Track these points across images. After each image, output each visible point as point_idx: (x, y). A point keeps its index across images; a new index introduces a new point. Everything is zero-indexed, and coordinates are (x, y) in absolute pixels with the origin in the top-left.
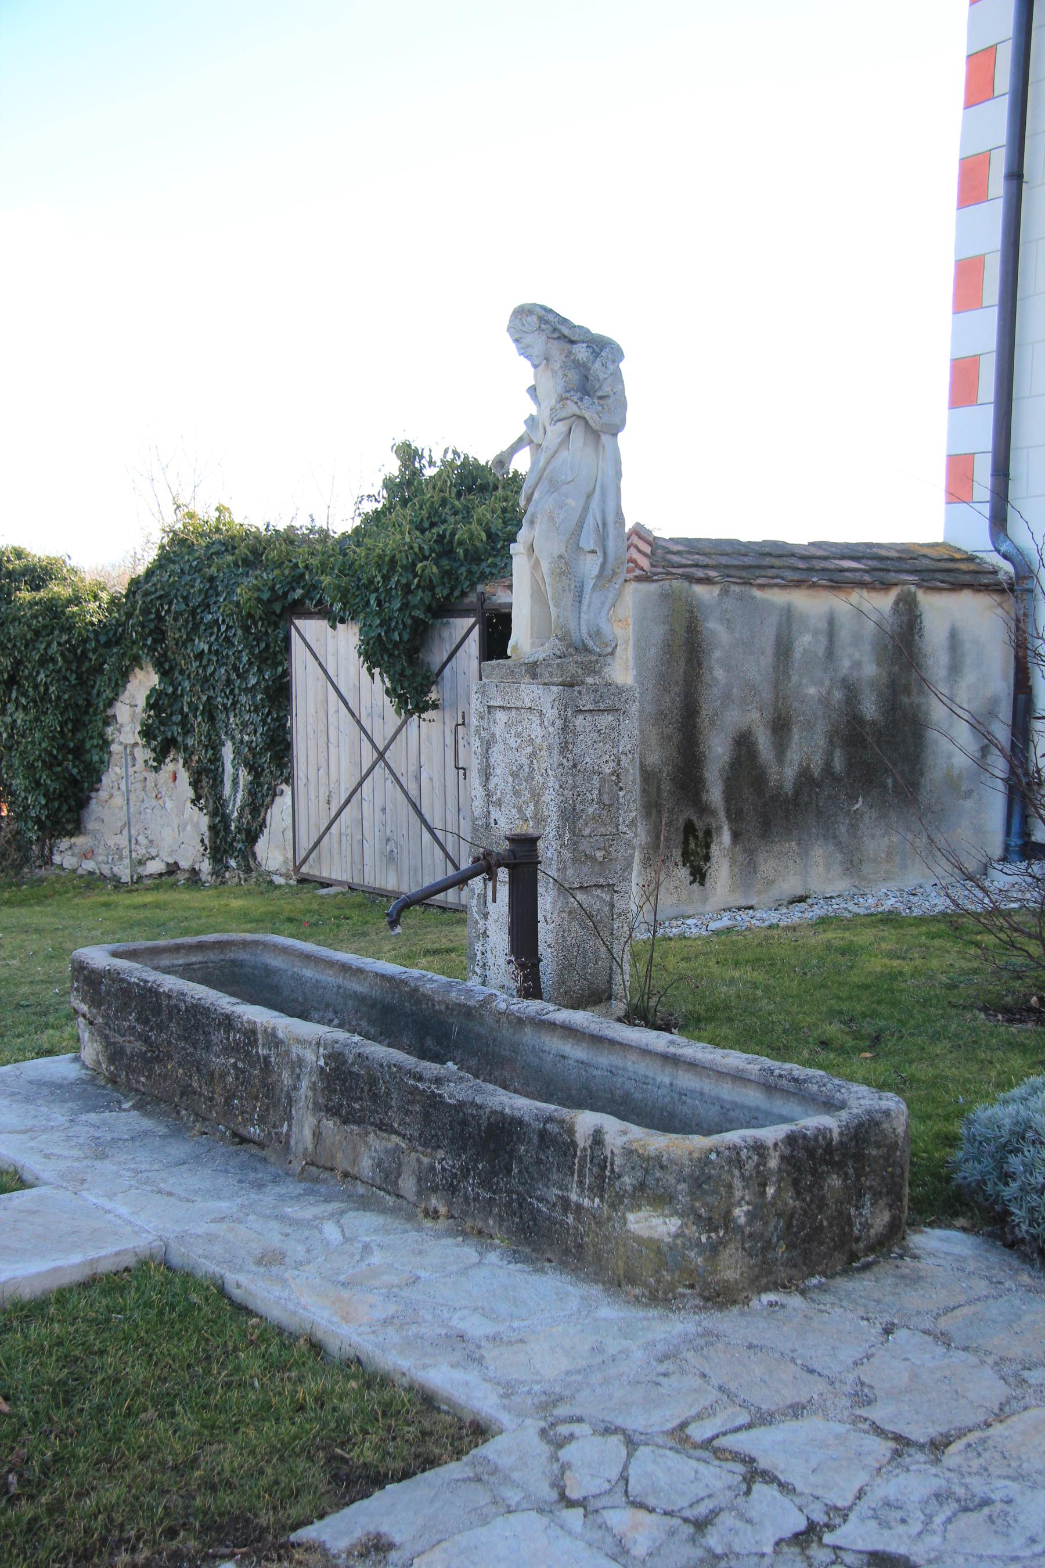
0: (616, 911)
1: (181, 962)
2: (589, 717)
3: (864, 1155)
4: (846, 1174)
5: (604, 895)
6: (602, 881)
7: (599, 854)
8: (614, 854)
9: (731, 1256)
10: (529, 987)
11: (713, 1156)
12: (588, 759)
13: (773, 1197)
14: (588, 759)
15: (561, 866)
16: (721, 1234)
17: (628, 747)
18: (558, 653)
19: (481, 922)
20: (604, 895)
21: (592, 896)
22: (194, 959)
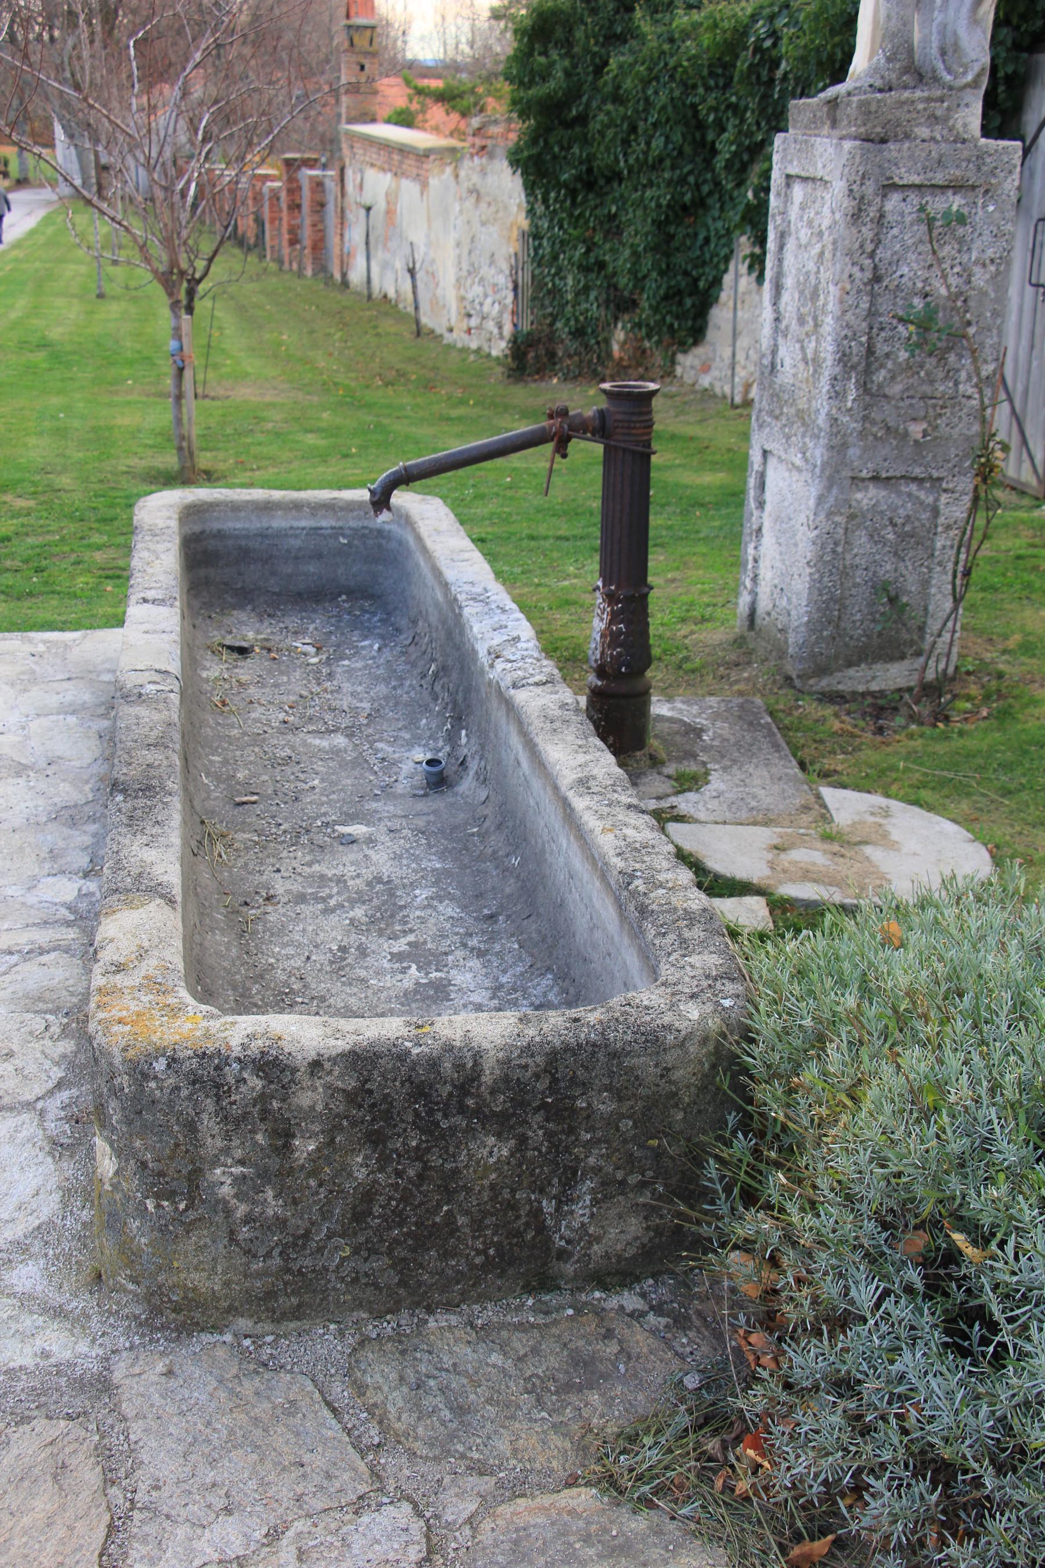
0: (941, 520)
1: (303, 523)
2: (914, 198)
3: (574, 1111)
4: (523, 1140)
5: (922, 495)
6: (918, 471)
7: (916, 430)
8: (944, 430)
9: (200, 1249)
10: (620, 632)
11: (160, 1065)
12: (905, 270)
13: (312, 1158)
14: (905, 270)
15: (836, 441)
16: (182, 1206)
17: (990, 253)
18: (878, 83)
19: (756, 513)
20: (922, 495)
21: (899, 493)
22: (324, 523)
